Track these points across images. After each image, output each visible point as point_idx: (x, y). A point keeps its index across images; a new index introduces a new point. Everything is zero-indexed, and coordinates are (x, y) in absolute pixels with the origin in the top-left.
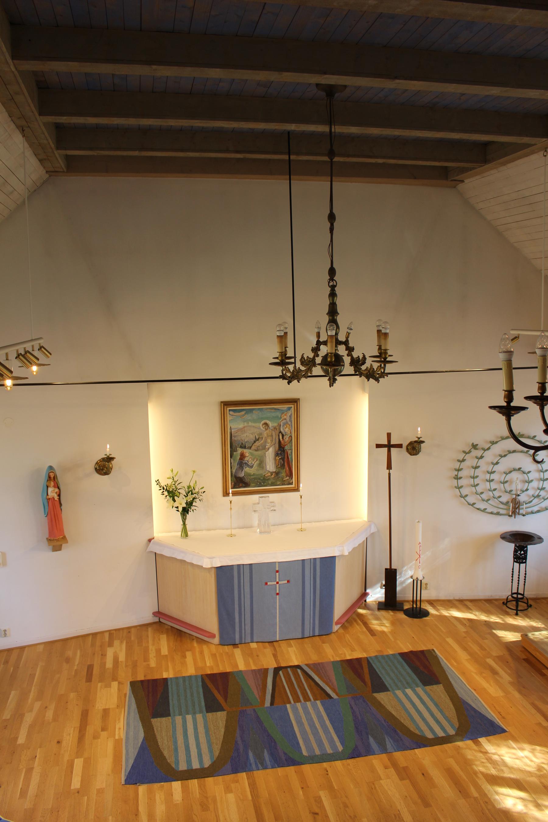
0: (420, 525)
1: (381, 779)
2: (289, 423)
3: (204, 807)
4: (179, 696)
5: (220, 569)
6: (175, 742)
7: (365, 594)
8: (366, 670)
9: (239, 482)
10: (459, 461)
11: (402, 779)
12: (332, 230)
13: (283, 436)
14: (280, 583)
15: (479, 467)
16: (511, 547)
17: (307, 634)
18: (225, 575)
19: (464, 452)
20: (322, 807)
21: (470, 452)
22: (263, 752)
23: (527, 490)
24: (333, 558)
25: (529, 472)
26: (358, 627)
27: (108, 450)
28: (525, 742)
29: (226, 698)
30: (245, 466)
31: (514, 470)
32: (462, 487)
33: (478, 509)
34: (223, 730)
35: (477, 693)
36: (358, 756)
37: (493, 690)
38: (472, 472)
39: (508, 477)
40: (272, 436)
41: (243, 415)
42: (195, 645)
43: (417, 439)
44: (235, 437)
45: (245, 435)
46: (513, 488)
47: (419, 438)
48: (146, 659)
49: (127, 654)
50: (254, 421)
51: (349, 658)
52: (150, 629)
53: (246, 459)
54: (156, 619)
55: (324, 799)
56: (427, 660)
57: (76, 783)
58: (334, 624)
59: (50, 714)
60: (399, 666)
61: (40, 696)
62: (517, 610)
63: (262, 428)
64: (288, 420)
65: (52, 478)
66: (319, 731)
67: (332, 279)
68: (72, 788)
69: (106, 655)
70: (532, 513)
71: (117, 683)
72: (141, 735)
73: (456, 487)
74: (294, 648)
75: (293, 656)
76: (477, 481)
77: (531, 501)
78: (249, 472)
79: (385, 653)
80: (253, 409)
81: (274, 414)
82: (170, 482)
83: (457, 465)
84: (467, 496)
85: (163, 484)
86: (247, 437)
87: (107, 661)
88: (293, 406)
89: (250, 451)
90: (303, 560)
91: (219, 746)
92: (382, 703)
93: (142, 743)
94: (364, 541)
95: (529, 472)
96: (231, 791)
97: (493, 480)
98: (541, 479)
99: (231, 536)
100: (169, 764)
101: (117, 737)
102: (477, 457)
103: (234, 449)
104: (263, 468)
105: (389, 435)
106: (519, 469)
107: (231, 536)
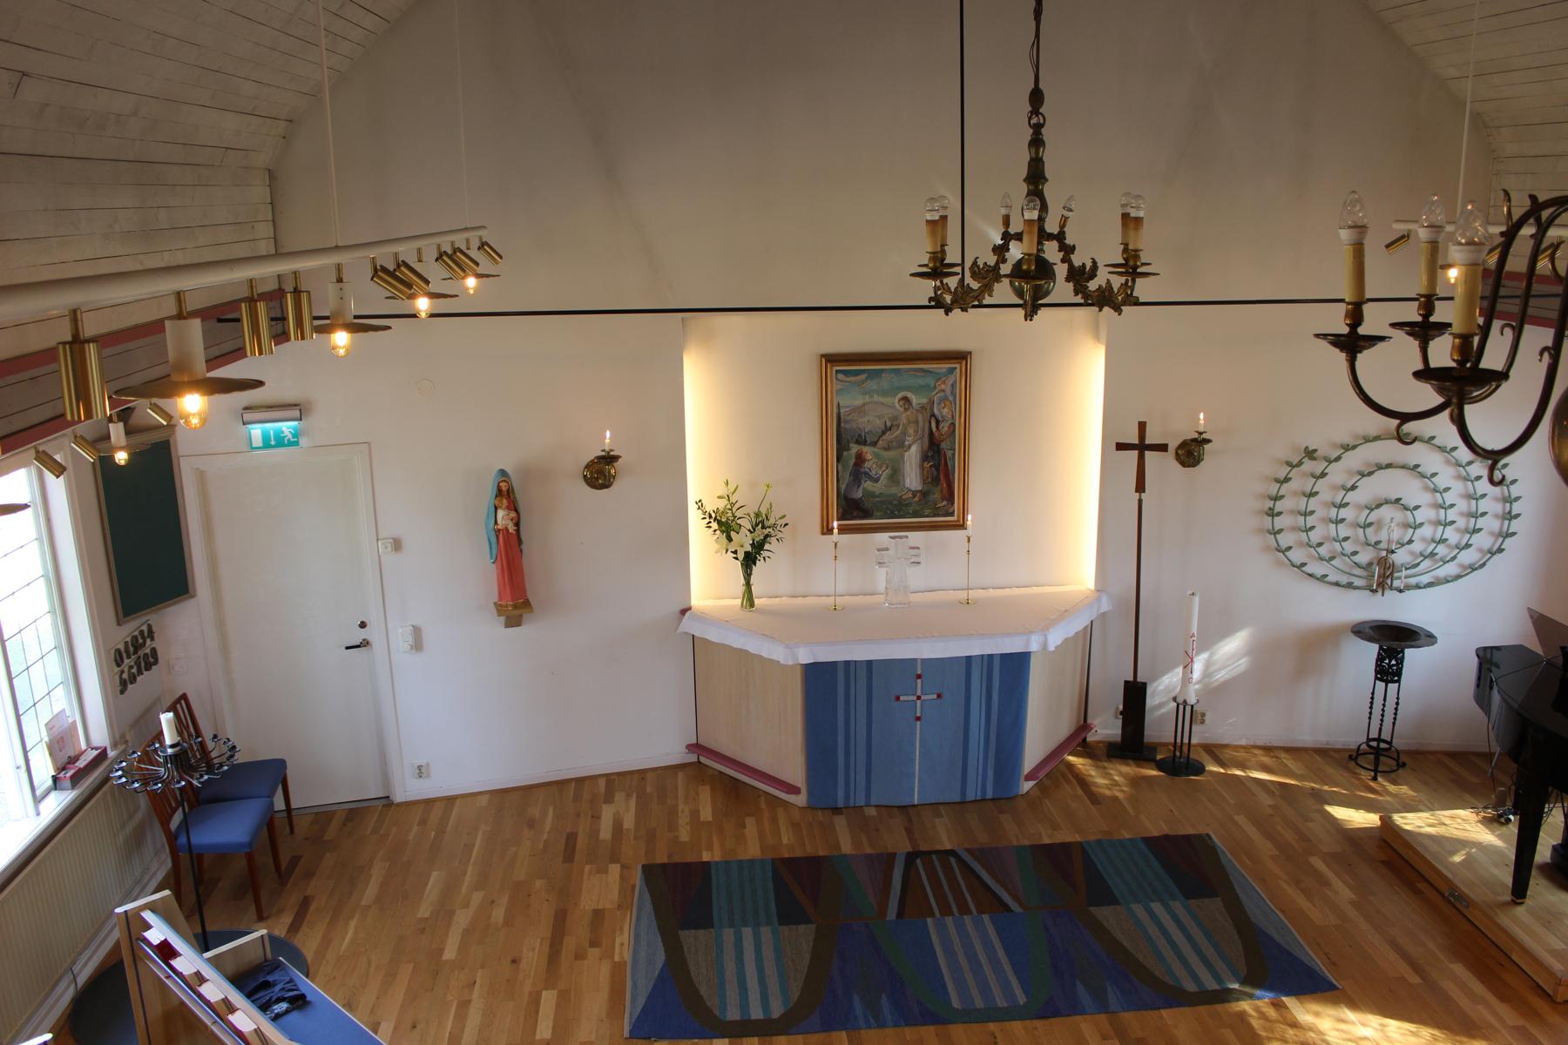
9: (854, 508)
13: (938, 422)
16: (1370, 652)
19: (1289, 464)
21: (1300, 463)
23: (1410, 542)
25: (1417, 507)
31: (1387, 502)
34: (807, 957)
36: (1056, 1014)
38: (1302, 503)
40: (917, 422)
46: (1383, 536)
50: (884, 393)
51: (1046, 841)
53: (867, 465)
54: (693, 758)
59: (498, 914)
65: (506, 494)
67: (1035, 111)
69: (599, 818)
70: (1418, 587)
72: (661, 957)
76: (1311, 521)
81: (921, 381)
82: (722, 504)
84: (1290, 548)
85: (709, 508)
86: (870, 422)
90: (969, 658)
95: (1417, 507)
97: (1343, 520)
101: (617, 959)
103: (846, 445)
104: (898, 483)
105: (1142, 426)
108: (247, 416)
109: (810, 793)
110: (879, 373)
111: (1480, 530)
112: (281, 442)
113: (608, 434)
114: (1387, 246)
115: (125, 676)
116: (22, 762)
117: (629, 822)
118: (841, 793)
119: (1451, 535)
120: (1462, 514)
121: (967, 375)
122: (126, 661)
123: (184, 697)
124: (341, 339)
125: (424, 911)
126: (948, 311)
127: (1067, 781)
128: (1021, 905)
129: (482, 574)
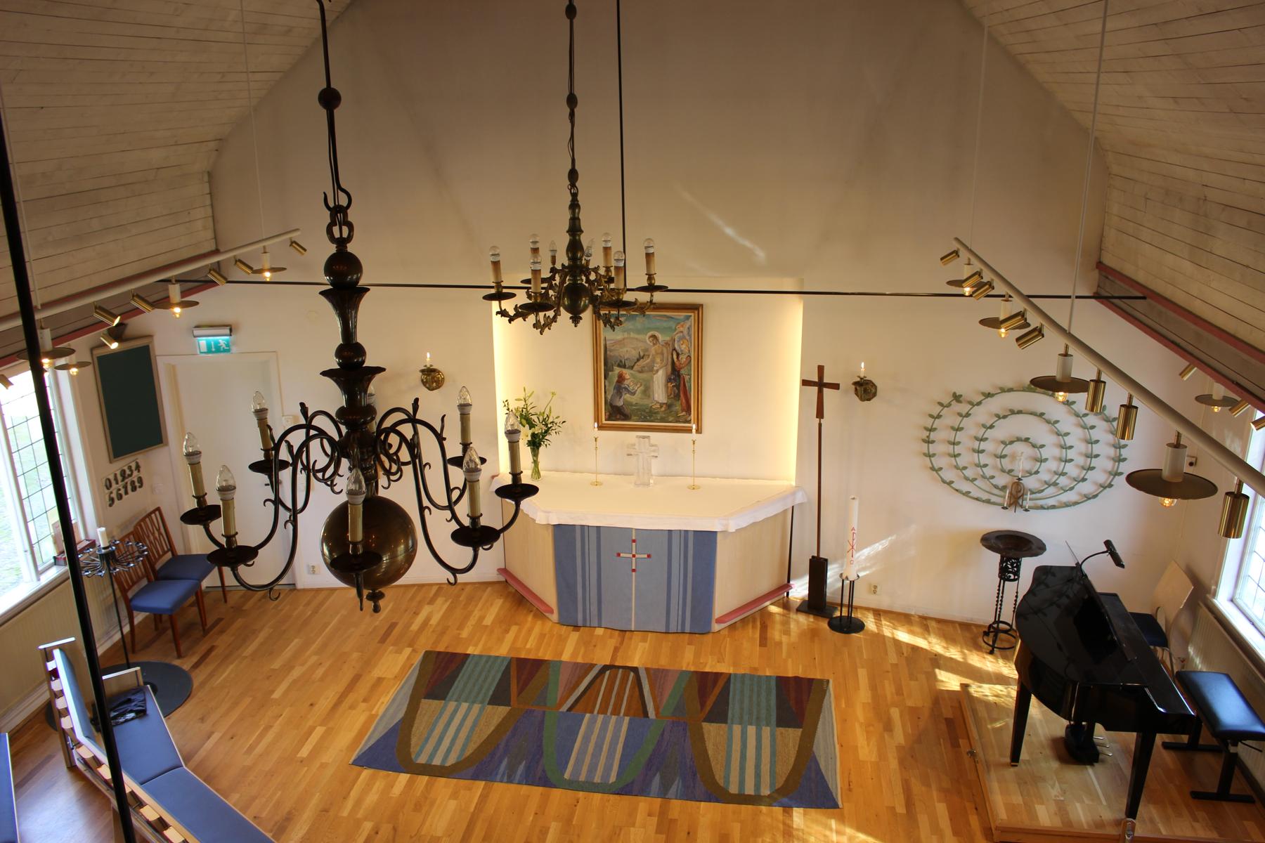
0: (856, 503)
1: (633, 825)
3: (418, 807)
5: (558, 528)
6: (432, 731)
7: (786, 587)
8: (717, 691)
9: (615, 413)
10: (931, 416)
11: (658, 831)
12: (572, 115)
13: (678, 355)
17: (673, 628)
18: (564, 535)
19: (941, 404)
21: (949, 405)
23: (1037, 472)
24: (713, 534)
25: (1042, 446)
30: (624, 392)
31: (1019, 439)
32: (934, 455)
34: (492, 728)
35: (841, 751)
37: (866, 750)
38: (951, 435)
39: (1008, 450)
42: (530, 618)
48: (461, 627)
50: (638, 332)
53: (626, 382)
55: (551, 831)
57: (304, 752)
59: (320, 672)
60: (764, 694)
62: (993, 647)
64: (686, 332)
67: (573, 185)
70: (1042, 508)
72: (401, 715)
74: (647, 645)
75: (638, 655)
76: (957, 449)
79: (760, 673)
82: (521, 404)
84: (941, 469)
86: (628, 352)
91: (479, 742)
92: (706, 736)
94: (785, 511)
95: (1042, 446)
96: (456, 798)
97: (983, 451)
98: (1061, 460)
99: (597, 484)
100: (409, 754)
105: (821, 369)
106: (1027, 440)
107: (597, 484)
108: (197, 332)
109: (560, 614)
110: (634, 317)
111: (1093, 468)
112: (218, 350)
115: (114, 495)
116: (28, 548)
117: (434, 621)
119: (1071, 469)
120: (1081, 454)
122: (114, 486)
123: (158, 509)
124: (177, 310)
125: (277, 664)
126: (511, 319)
127: (754, 627)
128: (657, 714)
129: (474, 414)
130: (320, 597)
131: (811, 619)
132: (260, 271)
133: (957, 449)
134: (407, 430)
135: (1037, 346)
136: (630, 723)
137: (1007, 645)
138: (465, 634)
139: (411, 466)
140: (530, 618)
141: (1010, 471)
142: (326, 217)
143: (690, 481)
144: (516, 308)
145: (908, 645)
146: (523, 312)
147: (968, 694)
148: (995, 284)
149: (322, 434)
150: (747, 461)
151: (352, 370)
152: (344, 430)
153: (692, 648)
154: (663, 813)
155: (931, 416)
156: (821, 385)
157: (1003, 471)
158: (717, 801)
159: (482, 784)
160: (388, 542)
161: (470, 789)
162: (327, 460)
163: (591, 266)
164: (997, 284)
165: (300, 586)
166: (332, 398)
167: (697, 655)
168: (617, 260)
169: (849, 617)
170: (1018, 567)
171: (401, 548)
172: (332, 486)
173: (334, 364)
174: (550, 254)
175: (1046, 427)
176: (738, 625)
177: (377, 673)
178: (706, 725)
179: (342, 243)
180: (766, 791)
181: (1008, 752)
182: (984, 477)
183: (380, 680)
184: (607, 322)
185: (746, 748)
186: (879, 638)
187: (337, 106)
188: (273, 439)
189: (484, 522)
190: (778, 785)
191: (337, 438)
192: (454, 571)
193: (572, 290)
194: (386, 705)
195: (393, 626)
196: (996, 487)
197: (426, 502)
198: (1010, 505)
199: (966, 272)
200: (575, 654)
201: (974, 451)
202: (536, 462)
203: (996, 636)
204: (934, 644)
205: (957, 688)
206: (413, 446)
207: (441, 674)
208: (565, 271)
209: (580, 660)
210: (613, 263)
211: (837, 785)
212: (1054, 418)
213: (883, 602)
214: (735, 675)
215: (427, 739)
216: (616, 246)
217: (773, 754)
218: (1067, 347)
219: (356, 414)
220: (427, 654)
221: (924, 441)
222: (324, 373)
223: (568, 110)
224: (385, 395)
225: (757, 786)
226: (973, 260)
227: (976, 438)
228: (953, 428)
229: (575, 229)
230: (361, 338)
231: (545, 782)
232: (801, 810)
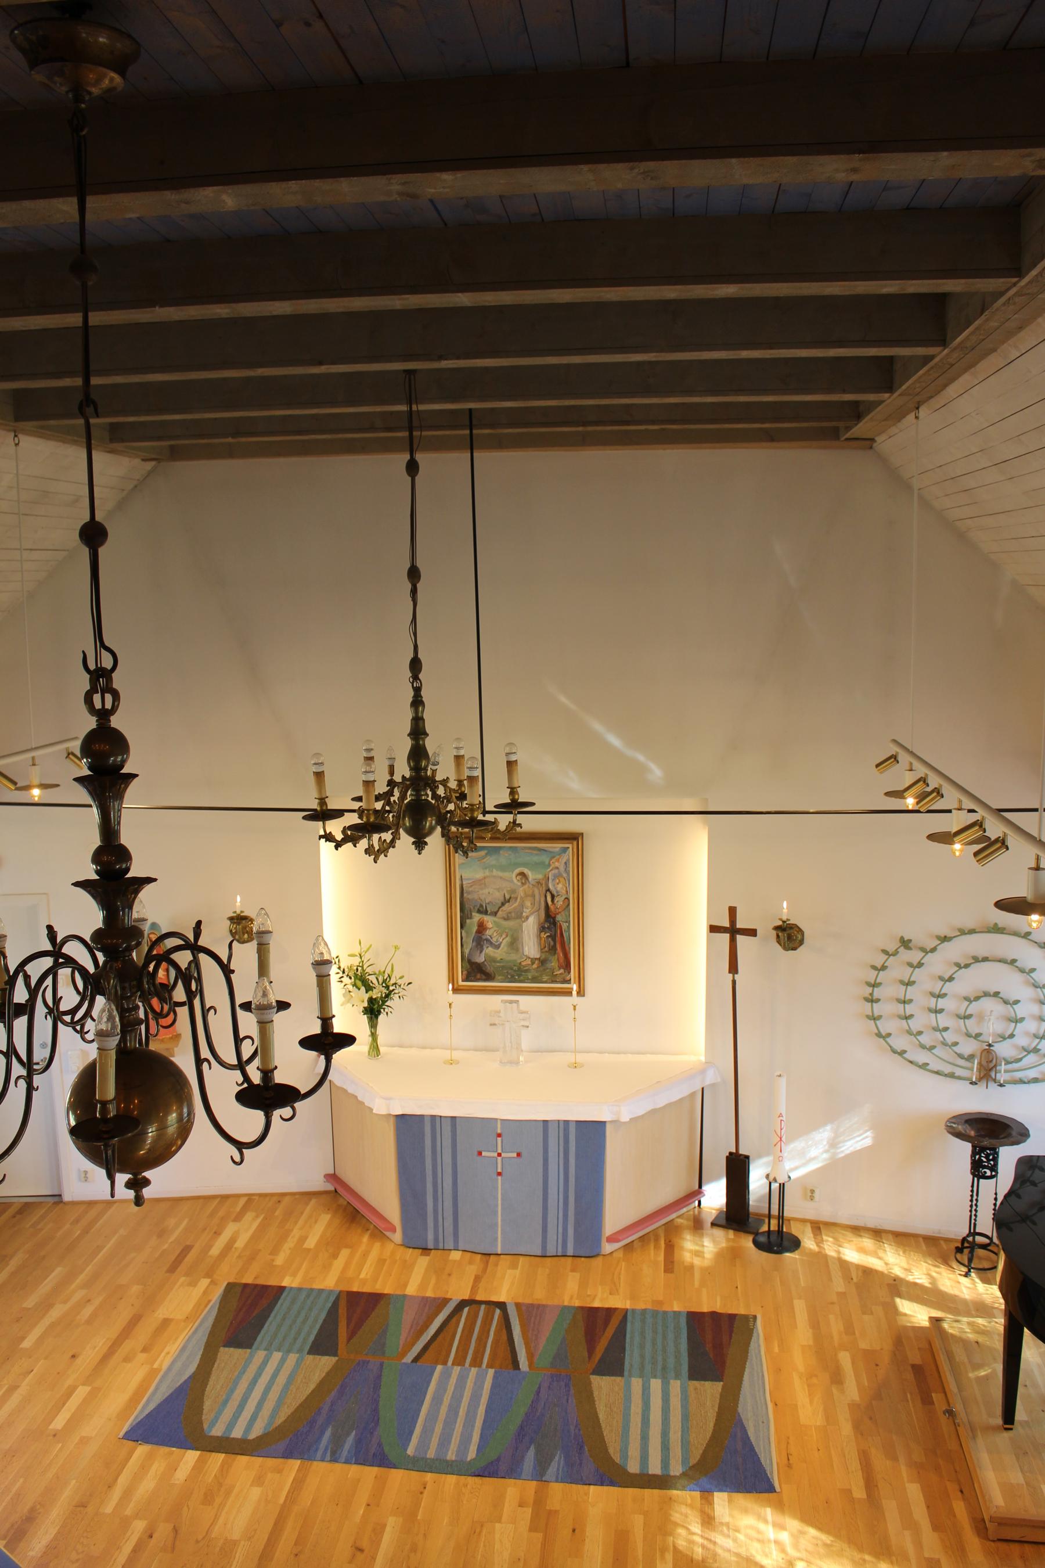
0: (783, 1082)
2: (565, 875)
3: (208, 1498)
4: (284, 1319)
8: (610, 1331)
9: (475, 972)
10: (874, 967)
11: (533, 1528)
12: (414, 592)
13: (553, 897)
14: (503, 1155)
15: (914, 982)
17: (551, 1250)
18: (410, 1129)
19: (885, 952)
20: (376, 1543)
21: (896, 953)
22: (348, 1434)
23: (1012, 1036)
24: (601, 1125)
25: (1017, 1002)
26: (652, 1252)
27: (238, 904)
28: (794, 1516)
29: (352, 1335)
31: (986, 994)
32: (880, 1017)
33: (911, 1062)
34: (312, 1386)
35: (774, 1412)
36: (490, 1475)
37: (809, 1411)
38: (900, 991)
40: (533, 896)
41: (483, 858)
42: (365, 1239)
43: (780, 923)
44: (469, 893)
45: (486, 891)
47: (784, 922)
48: (275, 1251)
49: (252, 1237)
50: (503, 868)
52: (313, 1201)
54: (330, 1187)
55: (388, 1529)
56: (731, 1332)
58: (604, 1240)
59: (87, 1311)
60: (671, 1336)
61: (87, 1285)
63: (515, 881)
64: (562, 869)
66: (459, 1420)
67: (415, 677)
68: (51, 1427)
69: (220, 1234)
70: (1021, 1081)
71: (209, 1280)
72: (192, 1369)
73: (868, 1017)
74: (517, 1272)
75: (506, 1286)
76: (909, 1009)
77: (1020, 1060)
78: (492, 954)
80: (500, 848)
81: (536, 859)
82: (356, 961)
83: (872, 975)
84: (889, 1035)
86: (490, 894)
87: (217, 1244)
88: (570, 846)
89: (495, 919)
91: (295, 1405)
92: (596, 1394)
93: (185, 1381)
94: (692, 1095)
95: (1017, 1002)
97: (941, 1011)
99: (451, 1062)
100: (201, 1422)
101: (155, 1366)
102: (910, 965)
104: (517, 950)
105: (732, 911)
106: (996, 994)
107: (451, 1062)
110: (497, 850)
113: (239, 899)
114: (877, 766)
117: (240, 1244)
118: (430, 1236)
121: (579, 856)
125: (30, 1302)
128: (531, 1365)
130: (93, 1213)
131: (731, 1234)
132: (27, 788)
133: (909, 1009)
134: (183, 958)
135: (1000, 861)
136: (495, 1377)
137: (986, 1265)
138: (280, 1260)
139: (186, 1008)
140: (365, 1239)
141: (978, 1035)
142: (84, 682)
143: (570, 1058)
144: (344, 831)
145: (858, 1267)
146: (352, 835)
147: (942, 1332)
148: (944, 791)
149: (70, 961)
150: (641, 1030)
151: (113, 880)
152: (101, 958)
153: (577, 1275)
154: (539, 1502)
155: (874, 967)
156: (733, 931)
157: (968, 1035)
158: (612, 1483)
159: (297, 1463)
160: (154, 1110)
161: (280, 1471)
162: (78, 998)
163: (438, 778)
164: (947, 789)
165: (67, 1198)
166: (86, 917)
167: (583, 1284)
168: (470, 768)
169: (780, 1232)
170: (995, 1159)
171: (173, 1117)
172: (82, 1033)
173: (90, 873)
174: (387, 763)
175: (1019, 977)
176: (636, 1245)
177: (162, 1313)
178: (596, 1381)
179: (103, 715)
180: (676, 1469)
181: (999, 1410)
182: (944, 1044)
183: (166, 1322)
184: (458, 847)
185: (650, 1409)
186: (820, 1258)
187: (102, 543)
188: (7, 970)
189: (279, 1078)
190: (693, 1461)
191: (92, 970)
192: (240, 1146)
193: (415, 807)
194: (172, 1357)
195: (187, 1249)
196: (961, 1056)
197: (205, 1053)
198: (980, 1079)
199: (909, 779)
200: (423, 1285)
201: (930, 1010)
202: (374, 1035)
203: (972, 1252)
204: (892, 1261)
205: (926, 1323)
206: (190, 977)
207: (247, 1313)
208: (407, 784)
209: (429, 1294)
210: (467, 773)
211: (772, 1460)
212: (1029, 965)
213: (820, 1209)
214: (633, 1310)
215: (226, 1402)
216: (470, 750)
217: (686, 1417)
218: (1038, 858)
219: (116, 936)
220: (230, 1287)
221: (867, 1000)
222: (77, 884)
223: (409, 586)
224: (154, 910)
225: (665, 1463)
226: (917, 765)
227: (932, 995)
228: (902, 982)
229: (418, 731)
230: (126, 838)
231: (382, 1461)
232: (724, 1495)
